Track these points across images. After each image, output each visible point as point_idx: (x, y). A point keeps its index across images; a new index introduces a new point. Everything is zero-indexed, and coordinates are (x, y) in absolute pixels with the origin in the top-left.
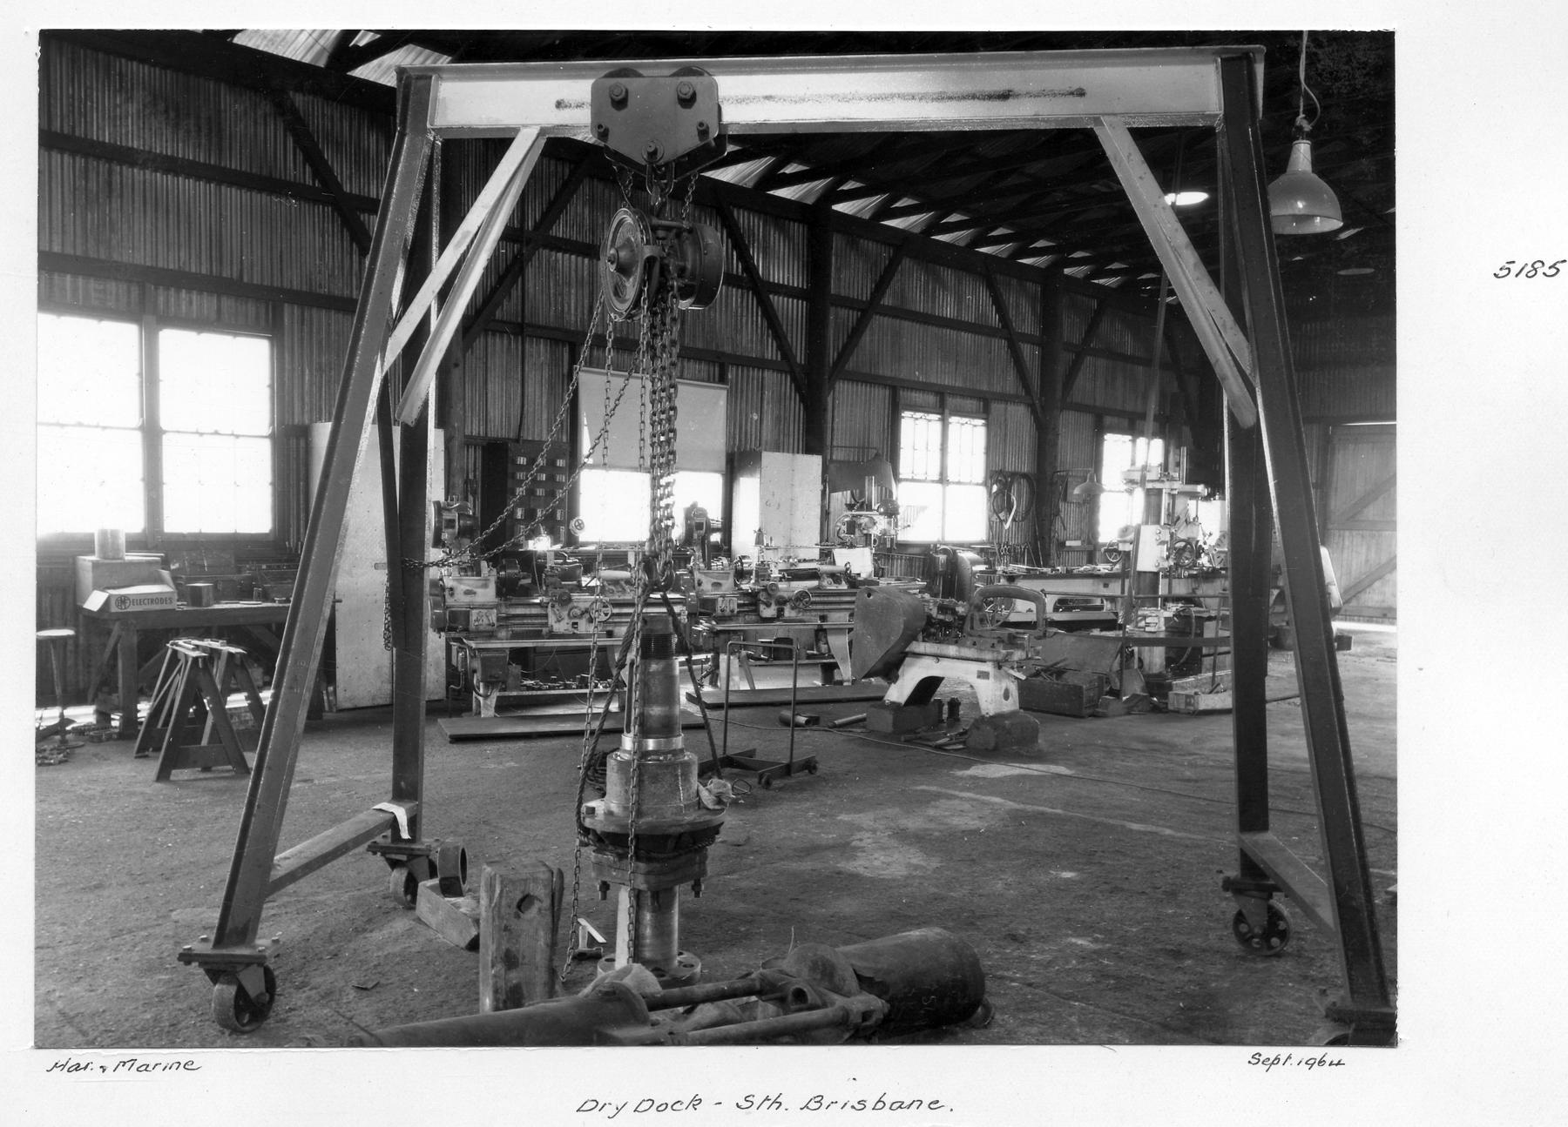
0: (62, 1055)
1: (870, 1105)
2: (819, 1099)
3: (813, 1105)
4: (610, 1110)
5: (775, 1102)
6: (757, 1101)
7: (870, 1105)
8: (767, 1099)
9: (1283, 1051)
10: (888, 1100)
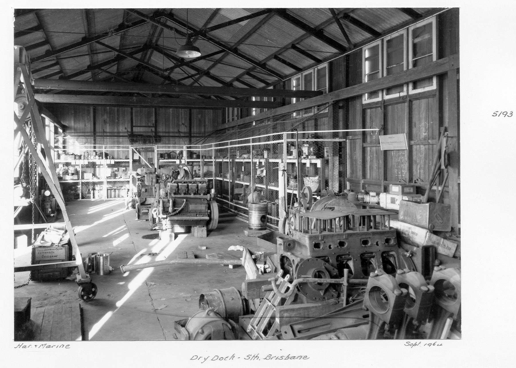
0: (21, 343)
4: (202, 360)
7: (284, 358)
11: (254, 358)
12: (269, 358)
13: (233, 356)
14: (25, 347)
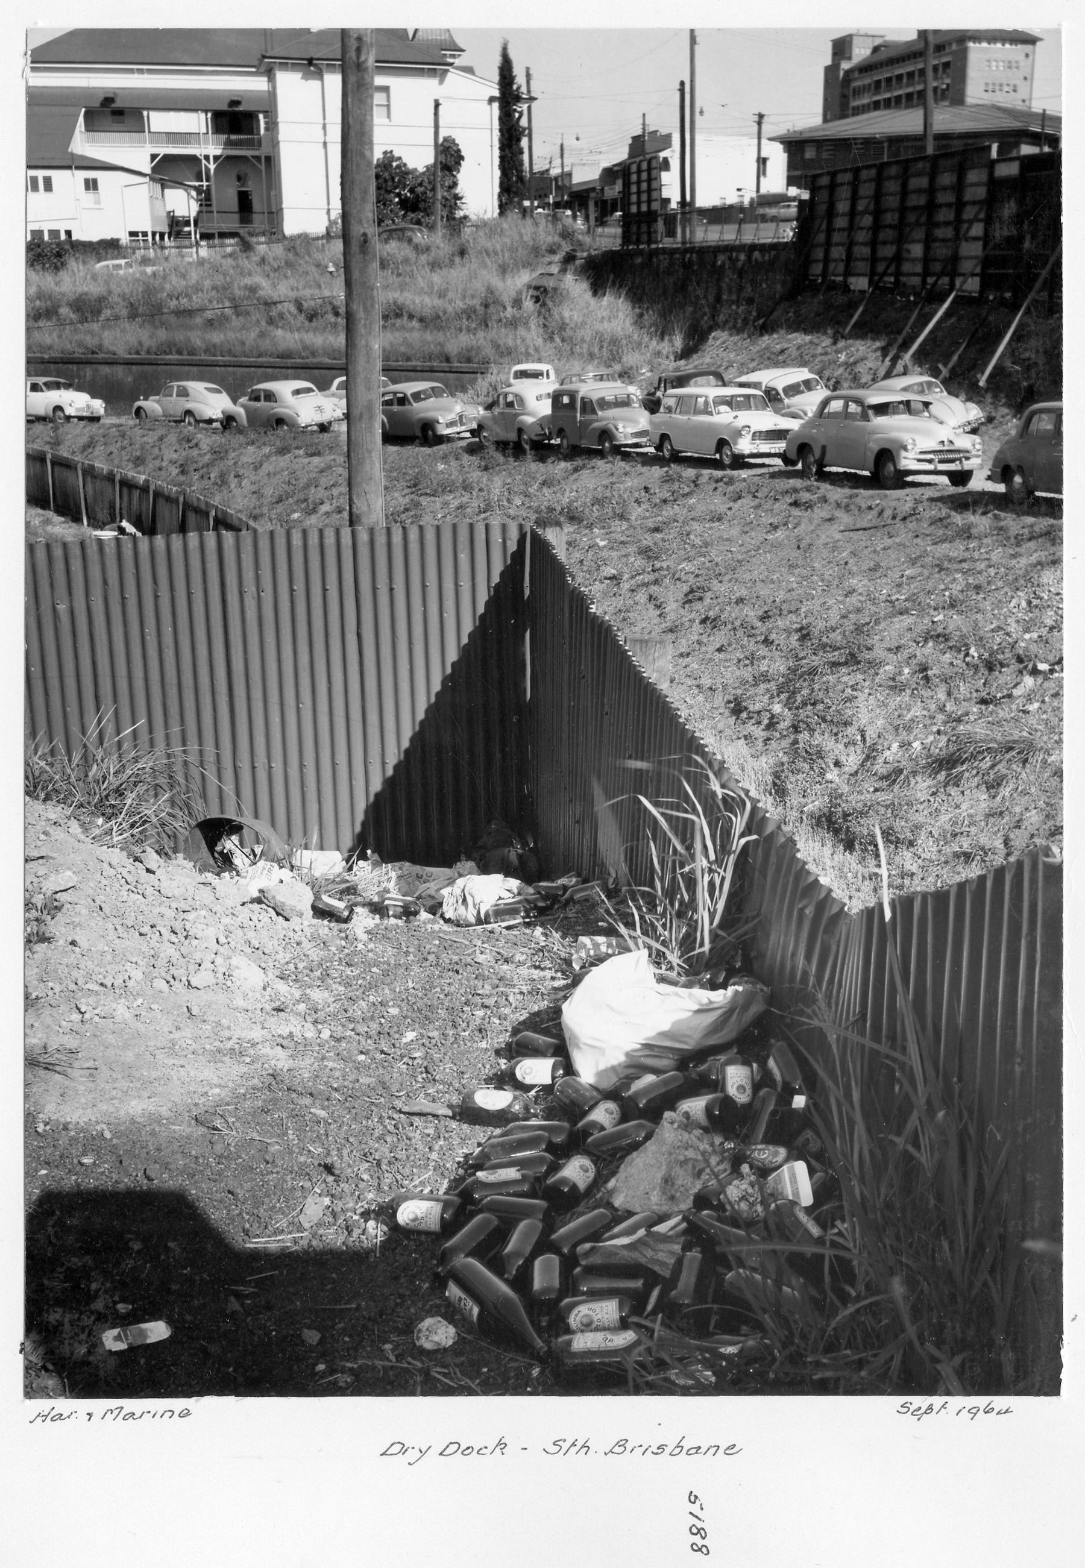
1: (668, 1450)
2: (622, 1443)
3: (617, 1449)
4: (412, 1455)
5: (583, 1446)
6: (565, 1446)
8: (574, 1445)
9: (937, 1401)
10: (687, 1445)
11: (574, 1449)
12: (622, 1449)
13: (502, 1445)
14: (185, 1414)
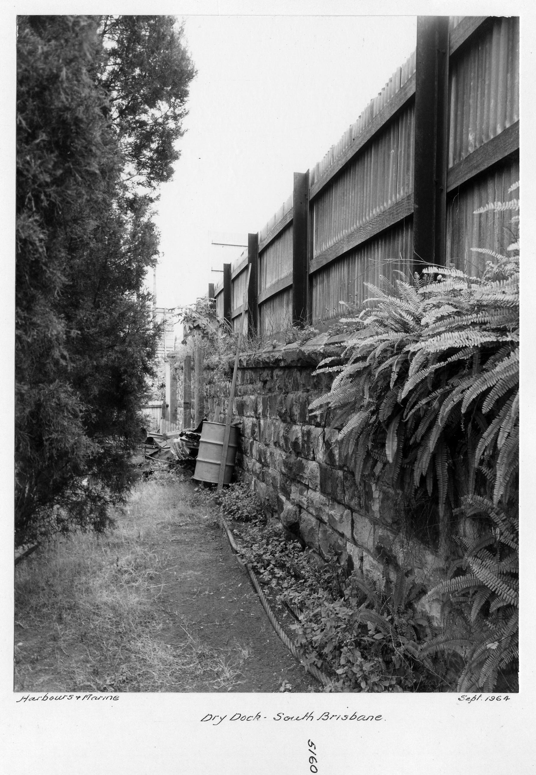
1: (349, 718)
4: (218, 720)
7: (349, 718)
9: (478, 694)
14: (116, 699)
